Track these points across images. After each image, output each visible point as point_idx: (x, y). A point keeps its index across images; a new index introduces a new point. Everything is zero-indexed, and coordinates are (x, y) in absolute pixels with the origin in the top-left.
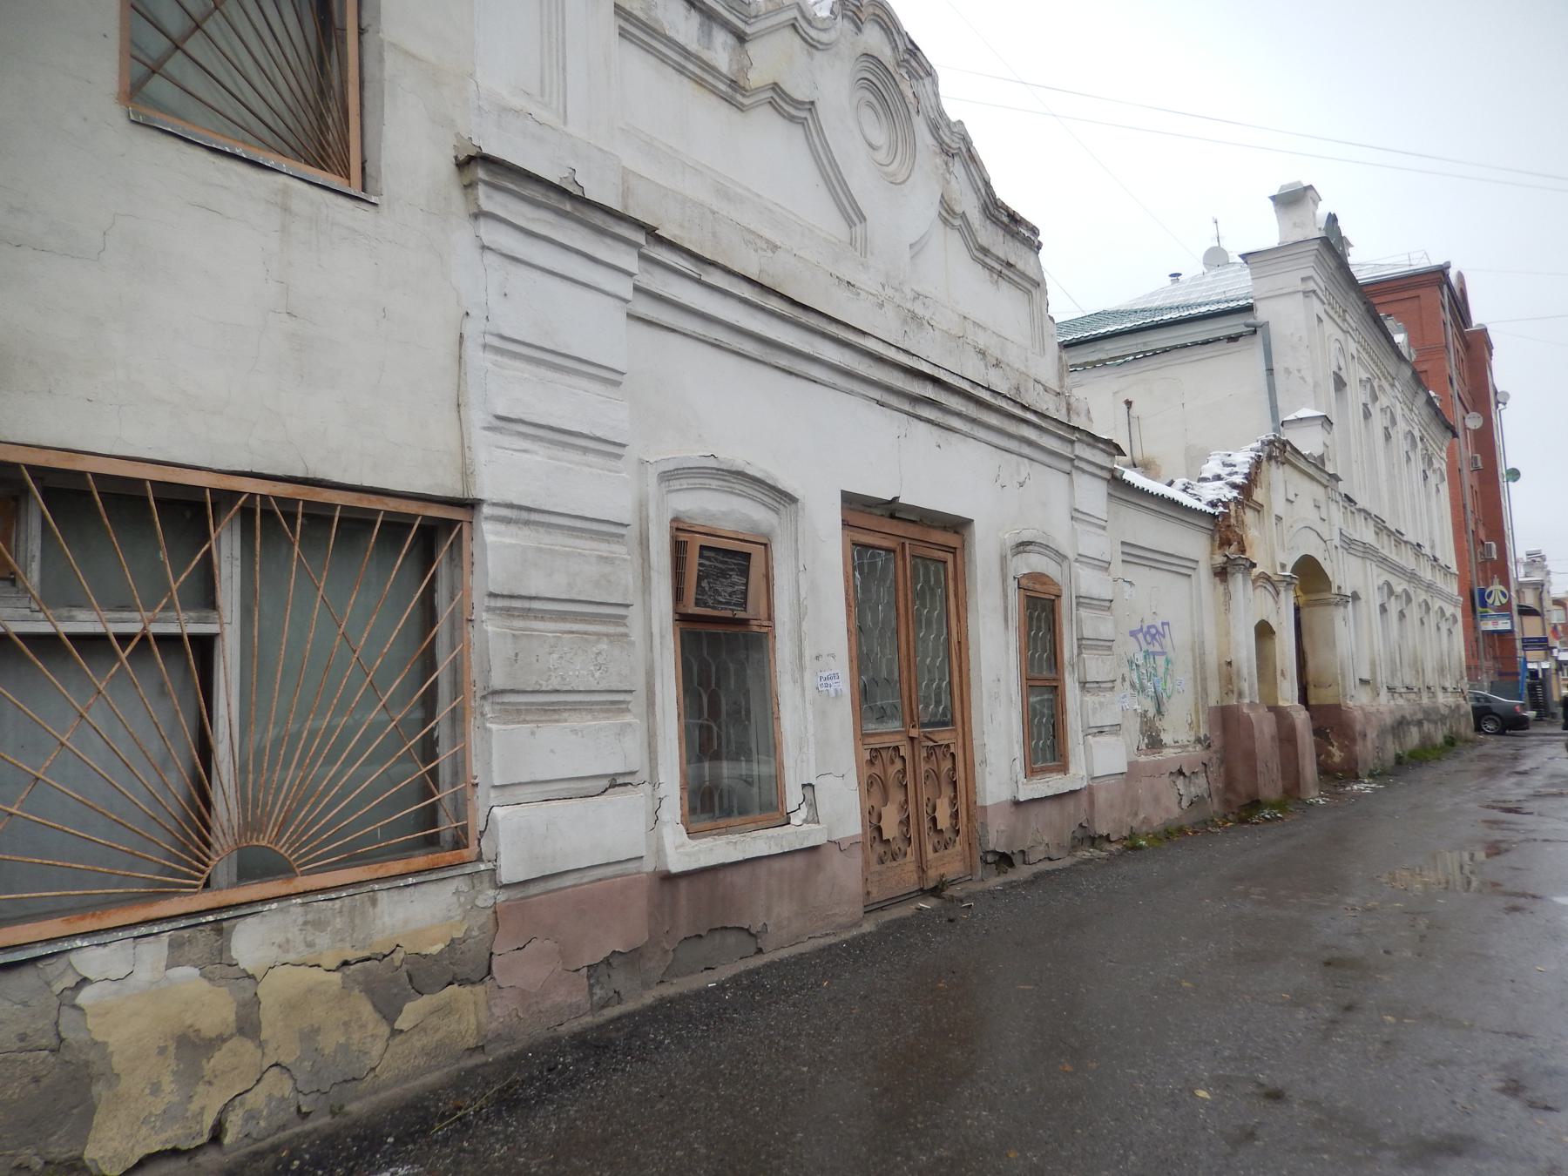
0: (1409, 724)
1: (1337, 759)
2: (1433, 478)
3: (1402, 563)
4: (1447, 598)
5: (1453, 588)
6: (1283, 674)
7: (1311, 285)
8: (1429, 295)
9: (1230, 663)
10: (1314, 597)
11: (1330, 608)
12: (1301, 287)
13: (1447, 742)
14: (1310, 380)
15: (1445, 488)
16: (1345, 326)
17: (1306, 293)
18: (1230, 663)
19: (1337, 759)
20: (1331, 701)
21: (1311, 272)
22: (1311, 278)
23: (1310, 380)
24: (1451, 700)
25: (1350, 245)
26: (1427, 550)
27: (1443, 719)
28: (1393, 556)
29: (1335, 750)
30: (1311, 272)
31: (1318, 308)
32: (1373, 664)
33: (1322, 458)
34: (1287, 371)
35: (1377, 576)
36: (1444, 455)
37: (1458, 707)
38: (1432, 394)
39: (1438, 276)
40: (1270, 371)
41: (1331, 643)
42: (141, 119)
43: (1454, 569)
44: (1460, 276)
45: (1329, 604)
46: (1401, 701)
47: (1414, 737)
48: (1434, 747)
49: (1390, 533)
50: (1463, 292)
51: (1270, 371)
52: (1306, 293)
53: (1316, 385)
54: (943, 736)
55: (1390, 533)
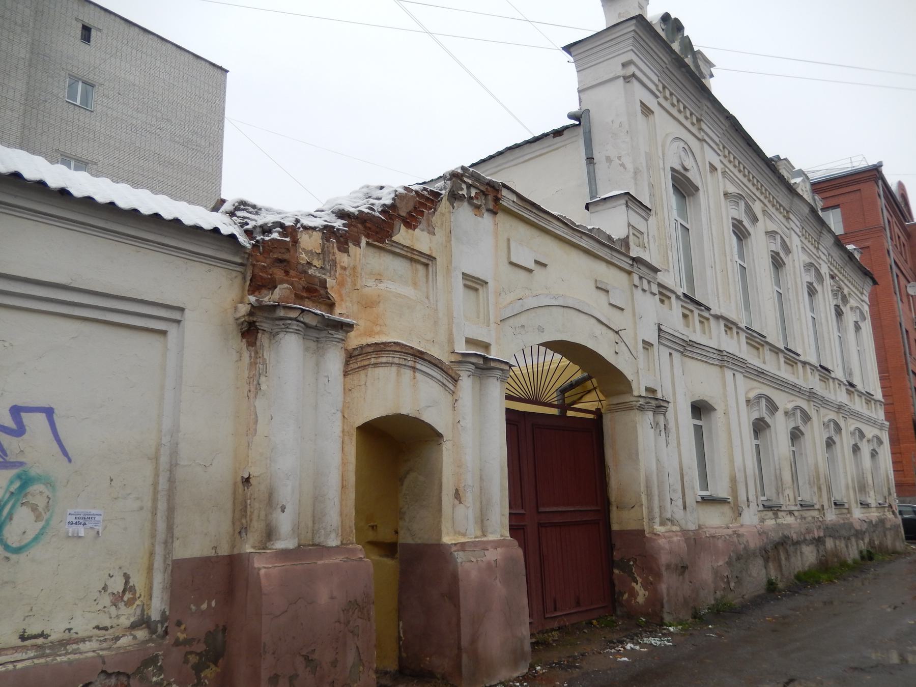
0: (797, 543)
1: (641, 599)
2: (850, 318)
3: (800, 382)
4: (873, 422)
5: (880, 414)
6: (457, 495)
7: (632, 69)
8: (866, 188)
9: (247, 481)
10: (615, 400)
11: (632, 413)
12: (620, 71)
13: (862, 558)
14: (630, 167)
15: (867, 327)
16: (701, 135)
17: (627, 79)
18: (247, 481)
19: (641, 599)
20: (633, 526)
21: (631, 56)
22: (631, 62)
23: (630, 167)
24: (874, 515)
25: (710, 64)
26: (838, 373)
27: (859, 534)
28: (791, 378)
29: (638, 587)
30: (631, 56)
31: (641, 94)
32: (733, 481)
33: (625, 242)
34: (609, 159)
35: (745, 387)
36: (867, 299)
37: (882, 521)
38: (850, 247)
39: (874, 174)
40: (590, 159)
41: (634, 456)
42: (281, 323)
43: (879, 395)
44: (901, 185)
45: (631, 408)
46: (789, 520)
47: (808, 556)
48: (843, 564)
49: (861, 394)
50: (904, 197)
51: (590, 159)
52: (627, 79)
53: (636, 172)
54: (534, 640)
55: (861, 394)
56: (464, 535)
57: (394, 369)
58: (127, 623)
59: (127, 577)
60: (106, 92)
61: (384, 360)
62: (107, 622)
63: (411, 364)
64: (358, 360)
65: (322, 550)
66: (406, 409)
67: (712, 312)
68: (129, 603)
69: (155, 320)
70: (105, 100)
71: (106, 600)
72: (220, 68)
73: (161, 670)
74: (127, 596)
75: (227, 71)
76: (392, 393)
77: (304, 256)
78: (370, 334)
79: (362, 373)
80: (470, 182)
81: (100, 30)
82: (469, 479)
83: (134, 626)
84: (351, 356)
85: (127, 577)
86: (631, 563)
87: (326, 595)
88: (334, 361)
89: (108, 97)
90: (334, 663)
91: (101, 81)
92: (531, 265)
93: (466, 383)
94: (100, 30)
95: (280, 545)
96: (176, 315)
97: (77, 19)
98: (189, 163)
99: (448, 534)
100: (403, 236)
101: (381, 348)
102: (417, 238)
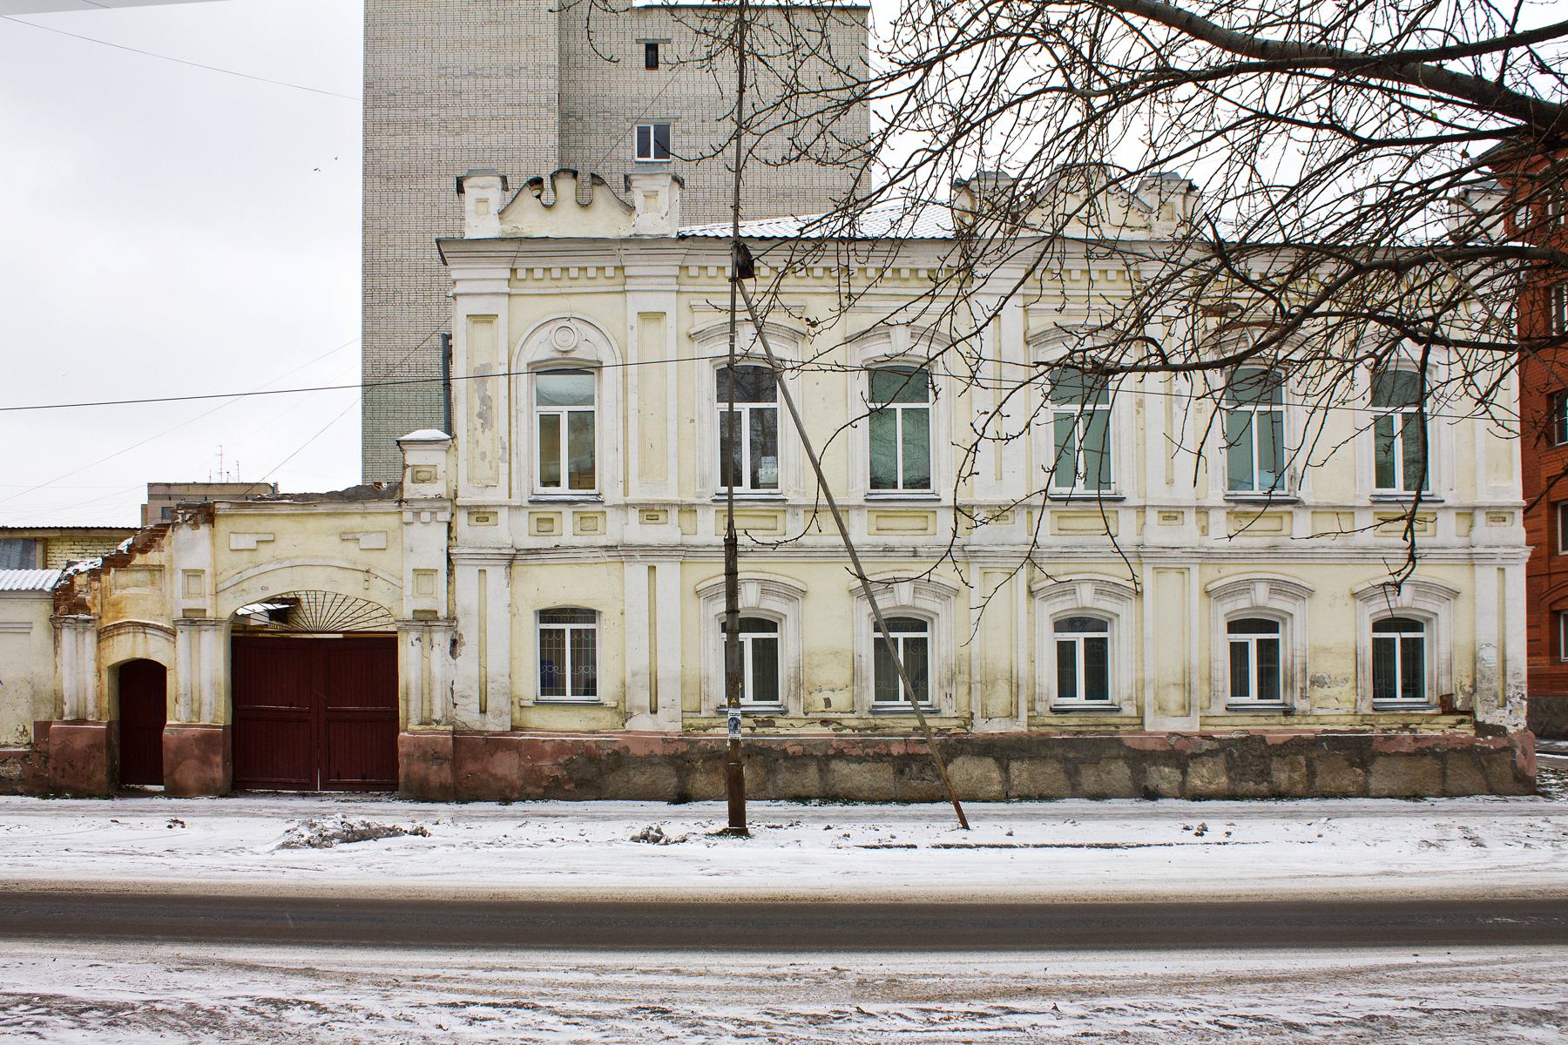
57: (603, 567)
60: (685, 127)
64: (103, 635)
65: (85, 721)
66: (140, 655)
69: (25, 628)
70: (685, 139)
72: (856, 8)
75: (867, 9)
76: (124, 649)
81: (669, 41)
84: (99, 634)
87: (80, 743)
88: (90, 638)
89: (689, 133)
91: (678, 113)
93: (182, 638)
94: (669, 41)
97: (638, 41)
98: (816, 183)
100: (139, 559)
101: (118, 626)
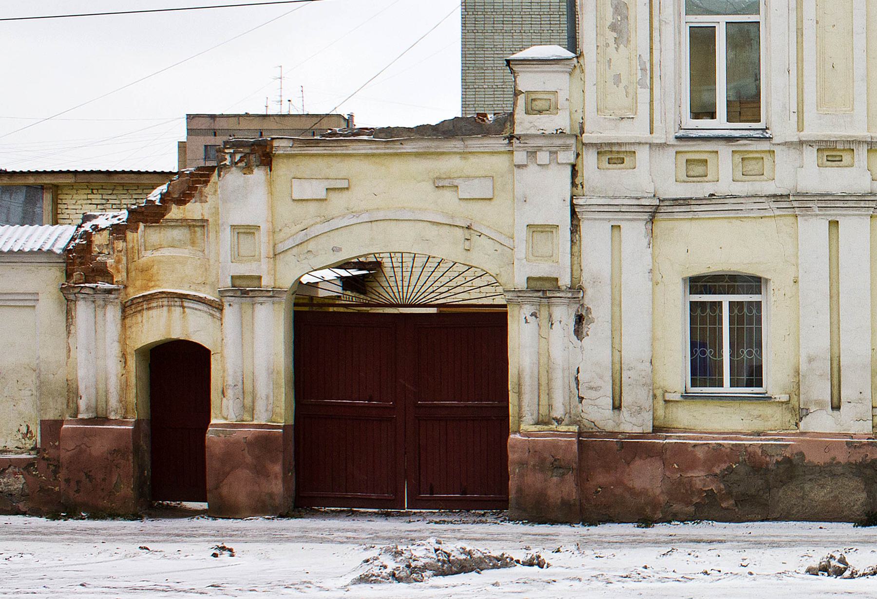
56: (226, 419)
58: (30, 447)
59: (28, 427)
61: (155, 305)
62: (21, 446)
63: (145, 307)
64: (130, 309)
67: (776, 140)
68: (30, 439)
71: (20, 436)
73: (36, 469)
74: (29, 435)
76: (157, 327)
77: (96, 249)
78: (147, 288)
79: (139, 315)
80: (232, 151)
82: (230, 381)
83: (32, 449)
84: (124, 308)
85: (28, 427)
86: (57, 444)
87: (99, 448)
88: (113, 313)
90: (104, 480)
92: (322, 194)
95: (80, 416)
96: (829, 159)
99: (216, 418)
102: (193, 210)
